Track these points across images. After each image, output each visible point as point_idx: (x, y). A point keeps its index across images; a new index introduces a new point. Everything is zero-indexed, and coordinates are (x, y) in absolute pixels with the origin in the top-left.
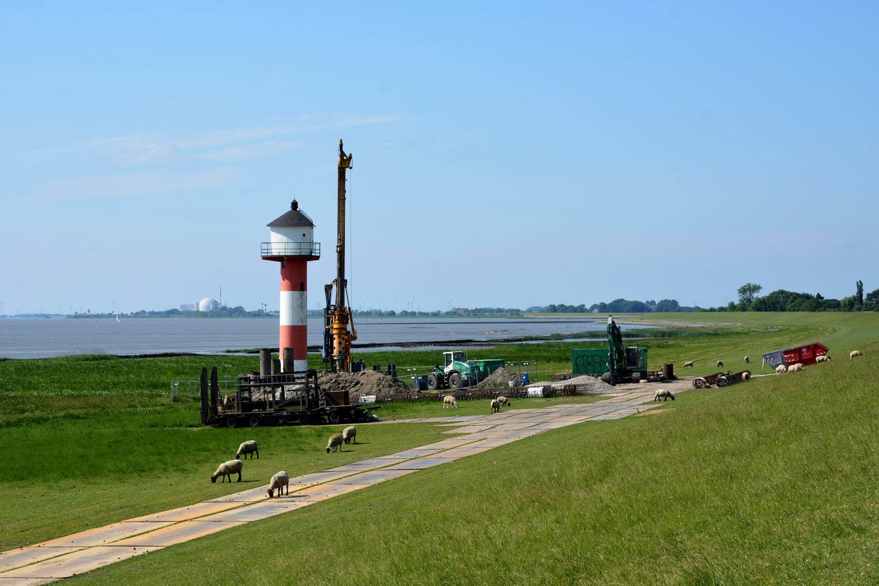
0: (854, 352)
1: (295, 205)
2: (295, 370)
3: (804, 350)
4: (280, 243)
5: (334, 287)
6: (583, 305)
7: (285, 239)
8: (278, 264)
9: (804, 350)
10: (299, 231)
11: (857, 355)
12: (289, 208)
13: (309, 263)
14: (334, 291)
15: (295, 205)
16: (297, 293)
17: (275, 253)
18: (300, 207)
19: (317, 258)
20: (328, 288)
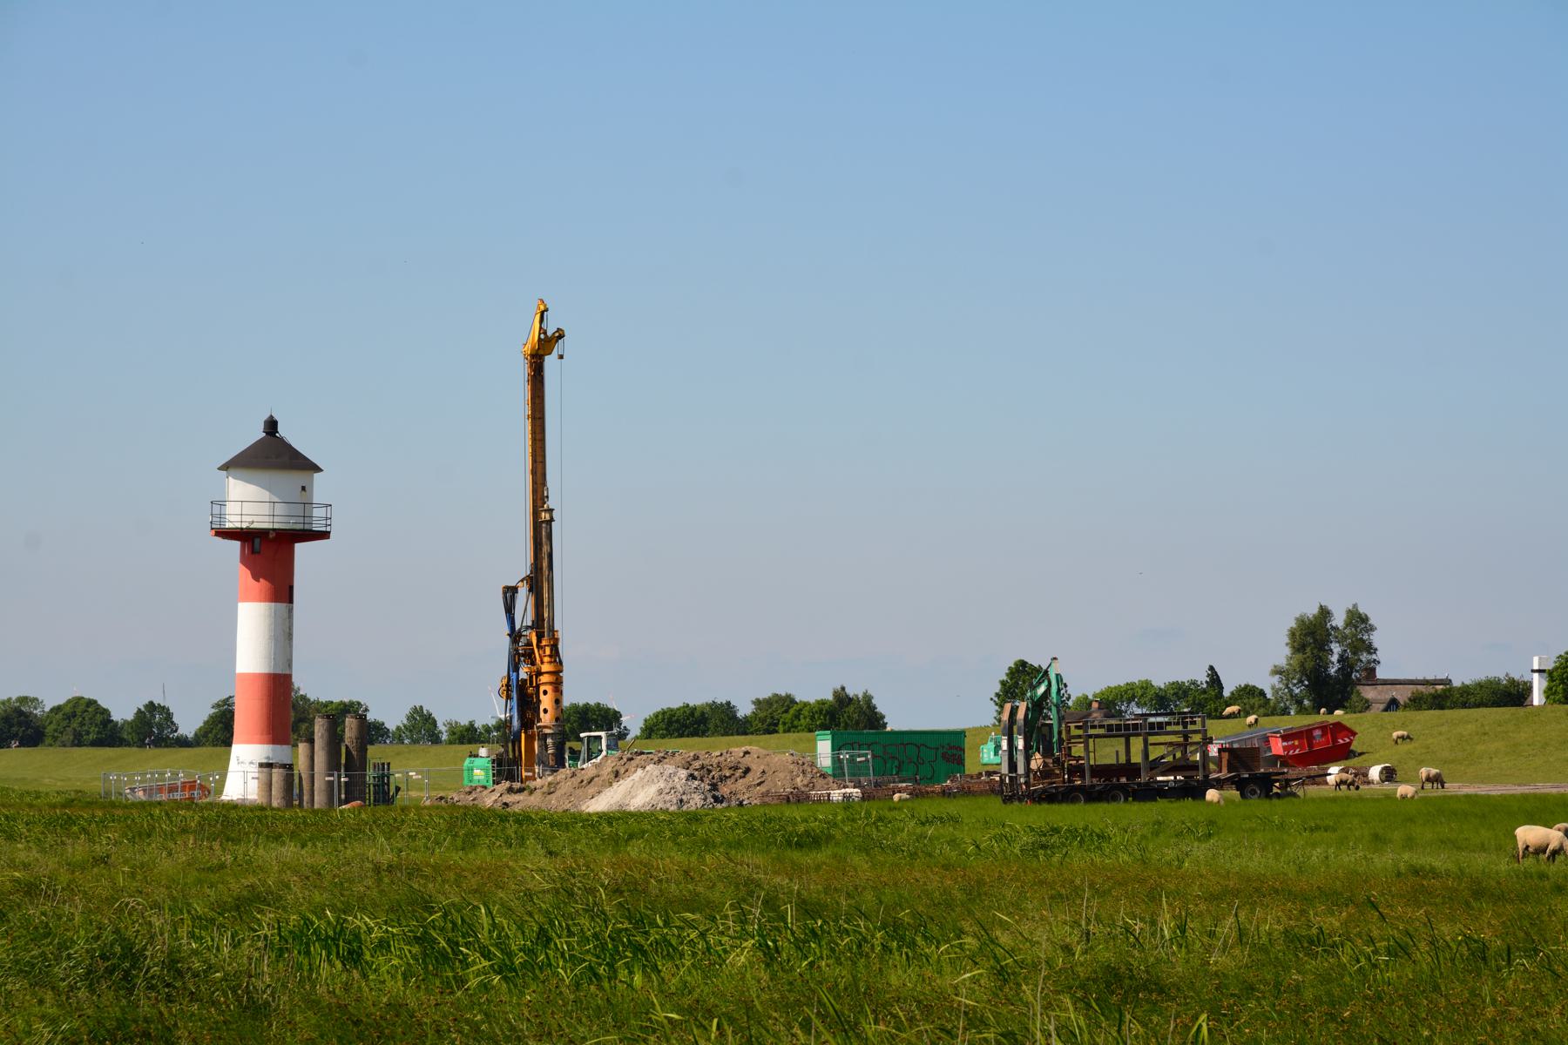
0: (1400, 733)
1: (271, 426)
2: (1381, 674)
3: (1317, 733)
4: (249, 503)
5: (523, 591)
6: (151, 703)
7: (265, 495)
8: (235, 545)
9: (1317, 733)
10: (290, 480)
11: (1402, 737)
12: (259, 434)
13: (299, 548)
14: (523, 600)
15: (271, 426)
16: (282, 606)
17: (233, 521)
18: (283, 431)
19: (324, 535)
20: (510, 593)
